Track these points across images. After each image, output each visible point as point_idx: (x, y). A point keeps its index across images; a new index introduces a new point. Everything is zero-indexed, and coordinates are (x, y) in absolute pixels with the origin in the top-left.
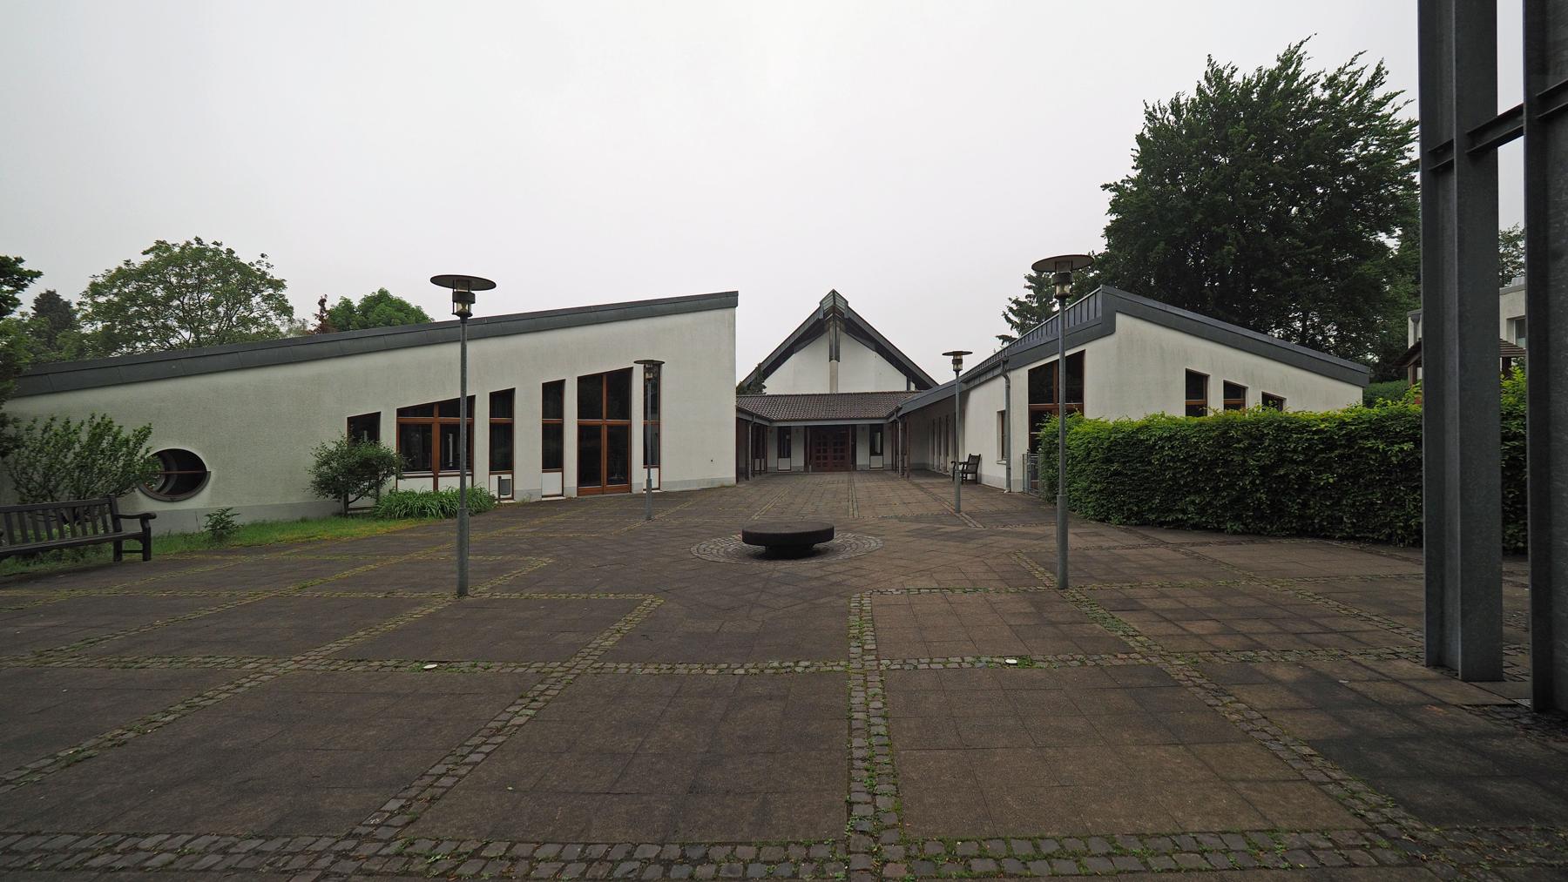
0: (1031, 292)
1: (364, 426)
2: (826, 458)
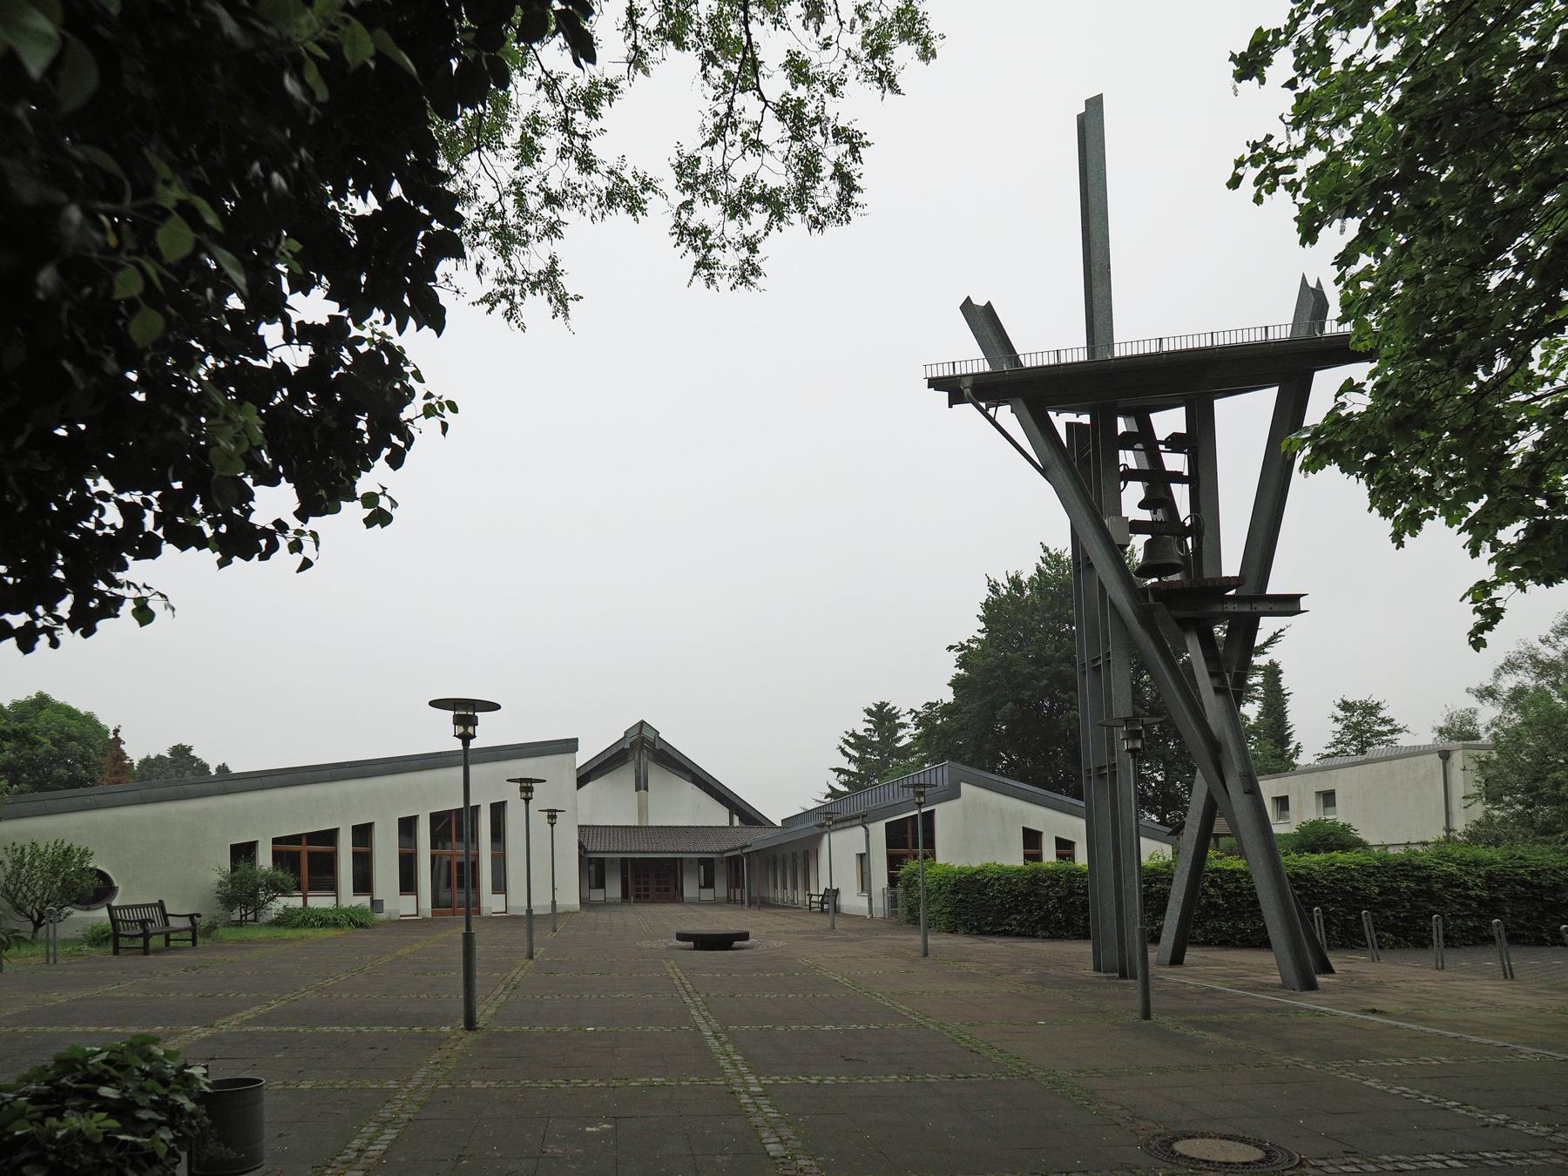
0: (871, 726)
1: (243, 852)
2: (646, 890)
